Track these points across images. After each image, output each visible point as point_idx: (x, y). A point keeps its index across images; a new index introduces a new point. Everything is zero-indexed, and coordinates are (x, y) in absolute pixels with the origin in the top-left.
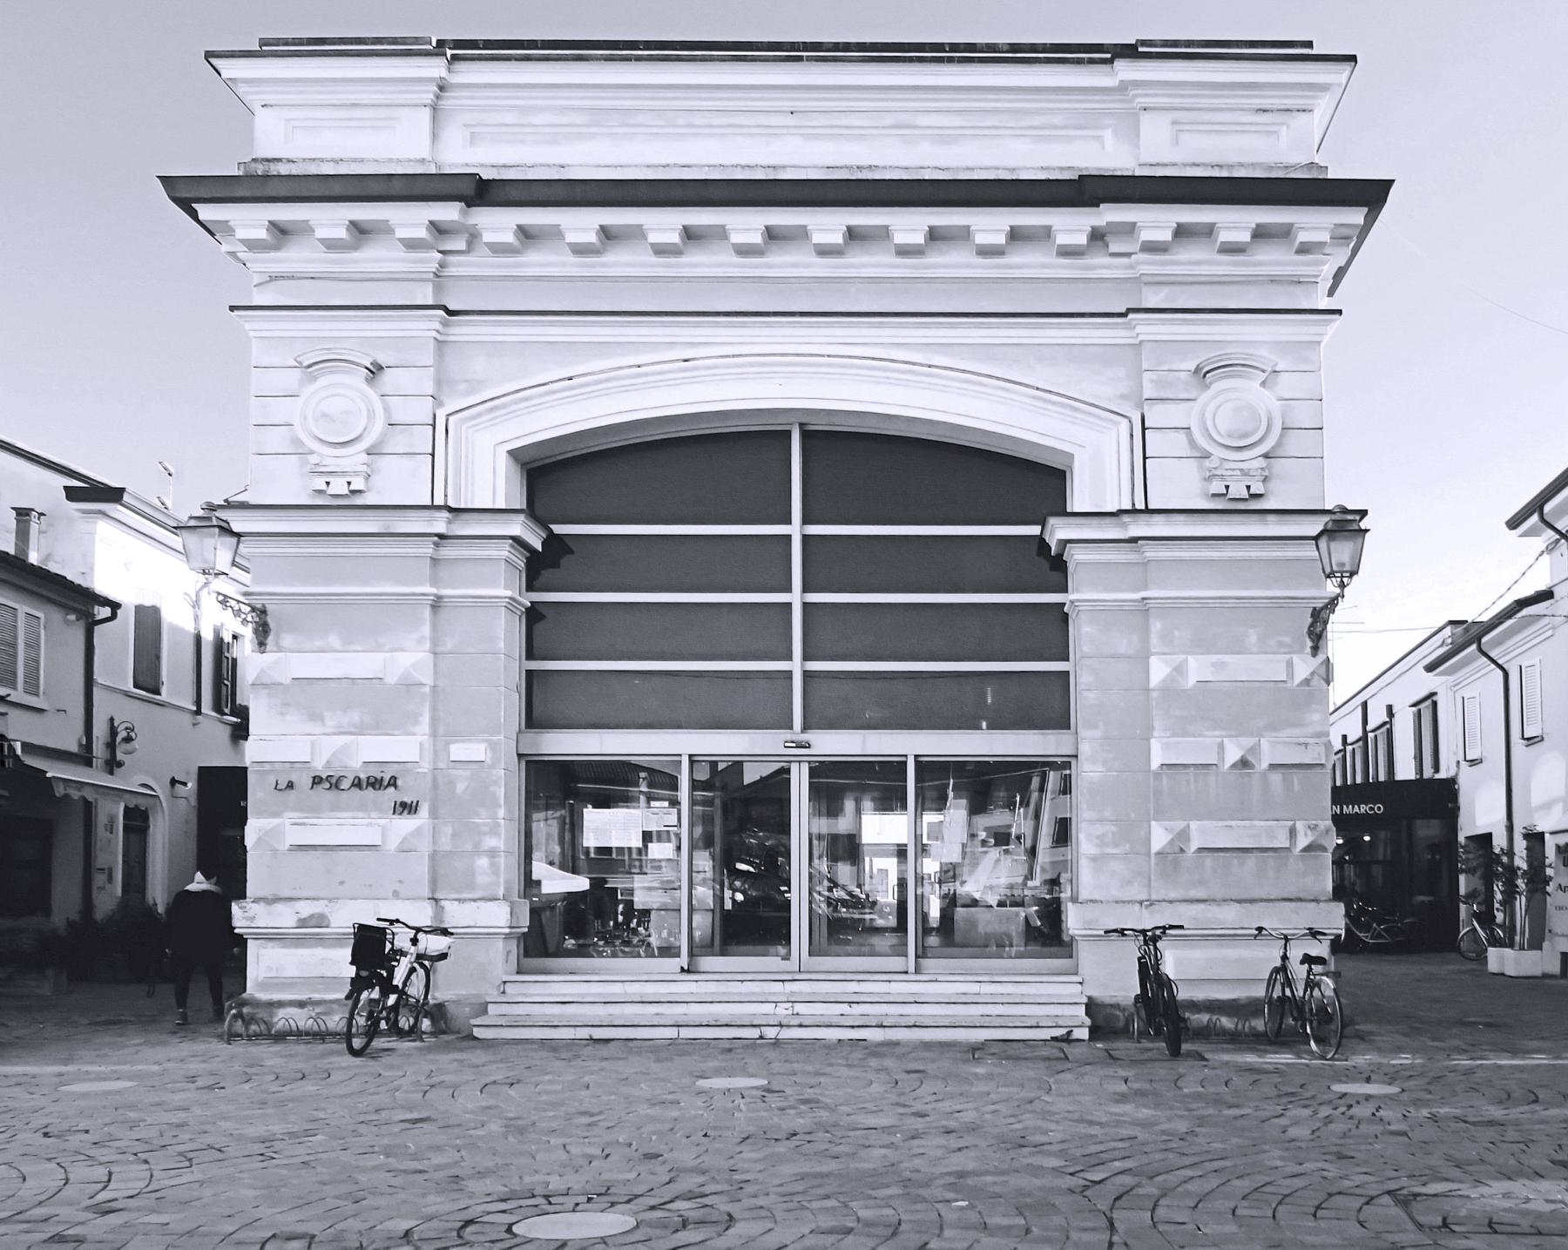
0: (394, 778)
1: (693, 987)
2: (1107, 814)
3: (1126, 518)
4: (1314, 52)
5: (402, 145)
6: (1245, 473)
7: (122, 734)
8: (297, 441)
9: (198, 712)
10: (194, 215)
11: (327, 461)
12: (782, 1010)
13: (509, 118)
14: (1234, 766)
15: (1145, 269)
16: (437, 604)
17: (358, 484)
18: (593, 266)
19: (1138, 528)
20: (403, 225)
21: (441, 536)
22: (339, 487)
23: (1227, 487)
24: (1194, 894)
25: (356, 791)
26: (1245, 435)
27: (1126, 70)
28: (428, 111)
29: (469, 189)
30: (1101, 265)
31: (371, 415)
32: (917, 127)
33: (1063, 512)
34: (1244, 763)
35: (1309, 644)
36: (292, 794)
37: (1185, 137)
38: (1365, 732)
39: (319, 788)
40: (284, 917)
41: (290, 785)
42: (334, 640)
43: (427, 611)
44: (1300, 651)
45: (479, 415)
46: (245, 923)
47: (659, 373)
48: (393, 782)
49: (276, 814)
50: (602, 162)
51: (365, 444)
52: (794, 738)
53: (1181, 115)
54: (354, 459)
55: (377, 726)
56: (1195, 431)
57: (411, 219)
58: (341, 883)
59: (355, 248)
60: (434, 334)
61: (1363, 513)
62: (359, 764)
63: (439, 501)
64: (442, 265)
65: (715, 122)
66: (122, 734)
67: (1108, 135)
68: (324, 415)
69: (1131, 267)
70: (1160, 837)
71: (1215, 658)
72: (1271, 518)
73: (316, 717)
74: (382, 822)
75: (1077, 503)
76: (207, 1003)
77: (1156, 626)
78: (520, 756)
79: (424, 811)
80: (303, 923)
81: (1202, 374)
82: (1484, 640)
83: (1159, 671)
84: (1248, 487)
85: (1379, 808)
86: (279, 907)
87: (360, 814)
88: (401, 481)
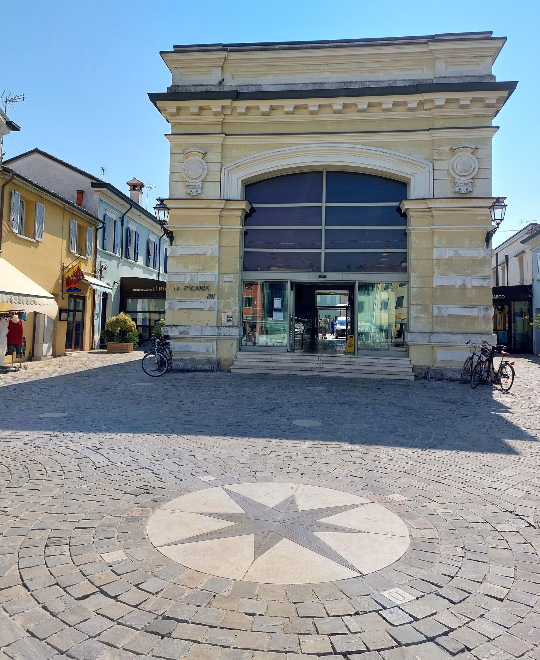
1: (291, 358)
2: (419, 302)
4: (493, 36)
6: (466, 184)
7: (104, 267)
9: (122, 258)
10: (156, 105)
17: (470, 189)
21: (222, 209)
25: (197, 292)
26: (466, 171)
27: (432, 46)
30: (422, 114)
31: (204, 168)
33: (406, 199)
36: (179, 291)
37: (449, 67)
38: (497, 266)
41: (178, 289)
42: (192, 242)
45: (234, 169)
47: (286, 154)
51: (201, 179)
52: (322, 274)
53: (448, 60)
54: (198, 182)
56: (450, 169)
57: (216, 105)
61: (505, 198)
65: (304, 69)
66: (104, 267)
67: (424, 67)
77: (436, 238)
79: (216, 298)
81: (452, 150)
83: (436, 254)
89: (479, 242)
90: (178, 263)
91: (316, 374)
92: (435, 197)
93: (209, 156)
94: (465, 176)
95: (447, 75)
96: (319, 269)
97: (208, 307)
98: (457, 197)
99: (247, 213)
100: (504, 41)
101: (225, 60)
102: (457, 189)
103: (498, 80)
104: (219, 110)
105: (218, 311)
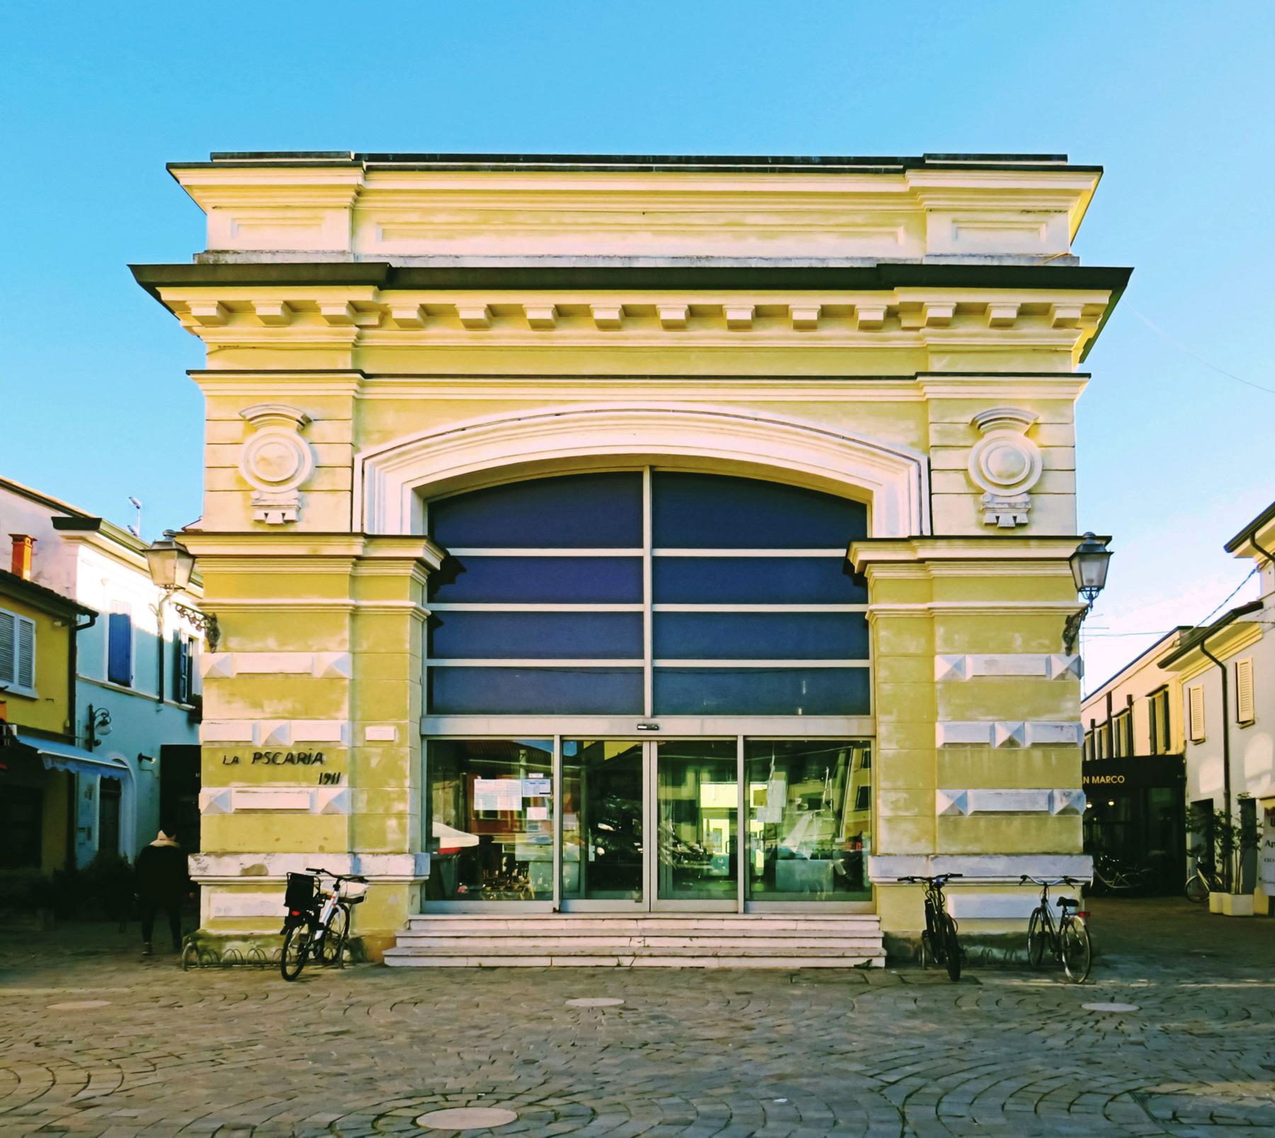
1: (563, 925)
2: (900, 784)
3: (915, 543)
5: (326, 239)
6: (1012, 506)
7: (99, 719)
8: (241, 480)
9: (161, 701)
10: (157, 296)
12: (635, 943)
13: (414, 217)
14: (1003, 745)
16: (355, 613)
17: (291, 515)
19: (925, 551)
21: (359, 558)
22: (275, 517)
24: (970, 848)
25: (289, 766)
26: (1012, 476)
27: (915, 179)
28: (347, 212)
29: (380, 275)
30: (895, 337)
31: (302, 458)
33: (863, 537)
34: (1011, 742)
35: (1064, 645)
37: (963, 233)
40: (231, 868)
41: (236, 760)
42: (271, 642)
43: (347, 620)
44: (1057, 651)
46: (199, 873)
47: (536, 425)
48: (319, 758)
49: (224, 784)
52: (646, 722)
53: (959, 215)
54: (288, 495)
55: (306, 712)
57: (334, 300)
58: (277, 840)
59: (289, 323)
60: (353, 393)
64: (359, 337)
66: (99, 719)
67: (901, 231)
68: (263, 459)
69: (919, 339)
70: (942, 803)
71: (987, 657)
72: (1033, 543)
73: (256, 705)
74: (311, 790)
75: (875, 531)
77: (940, 631)
78: (423, 736)
79: (344, 781)
80: (246, 872)
81: (977, 426)
82: (1207, 642)
83: (942, 667)
84: (1015, 518)
85: (1121, 779)
86: (226, 859)
87: (293, 784)
88: (327, 514)
89: (1047, 642)
90: (232, 695)
91: (627, 962)
92: (936, 533)
94: (1008, 486)
97: (319, 807)
98: (991, 534)
104: (343, 311)
105: (352, 818)
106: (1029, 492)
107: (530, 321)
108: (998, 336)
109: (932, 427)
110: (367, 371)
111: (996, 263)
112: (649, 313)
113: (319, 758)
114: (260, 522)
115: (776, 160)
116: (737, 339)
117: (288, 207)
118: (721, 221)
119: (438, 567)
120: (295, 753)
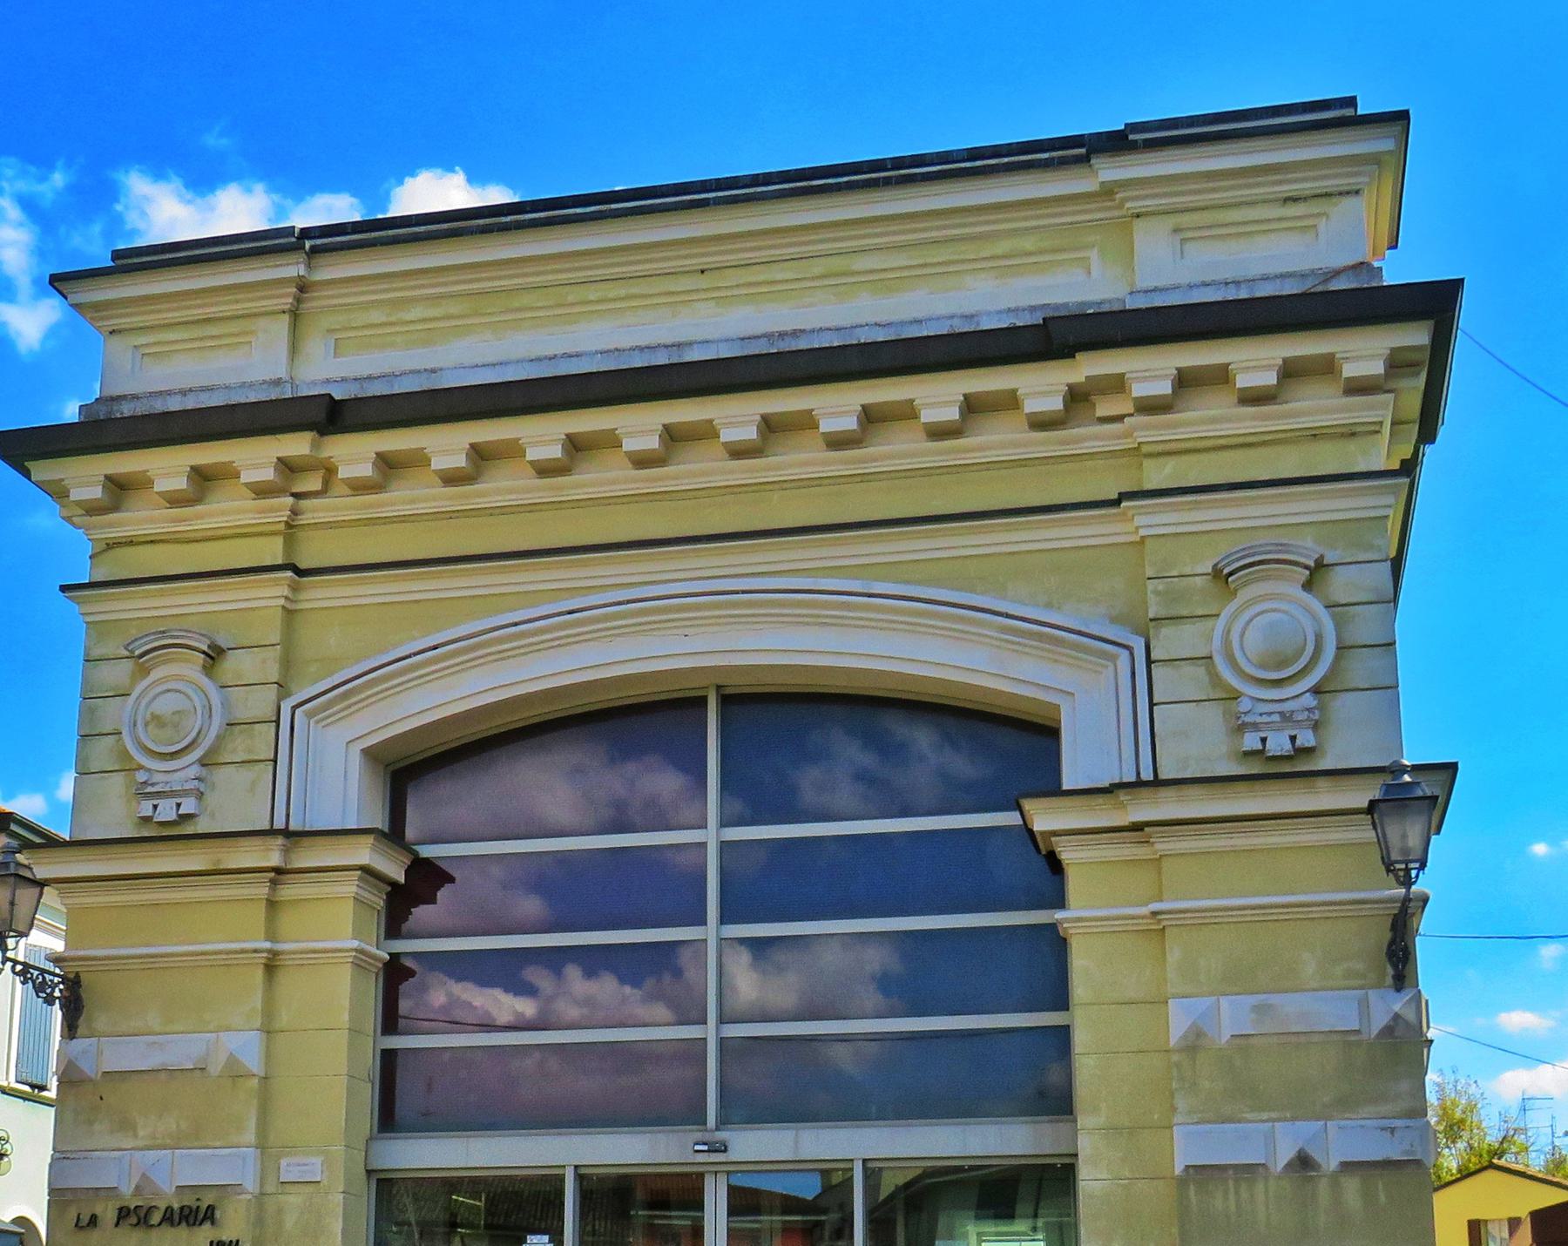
0: (211, 1208)
3: (1123, 796)
6: (1286, 717)
10: (27, 474)
11: (157, 778)
14: (1289, 1166)
15: (1141, 437)
17: (1306, 739)
18: (655, 480)
20: (630, 435)
21: (278, 871)
22: (167, 811)
23: (1264, 740)
27: (1109, 170)
28: (286, 317)
29: (320, 414)
30: (1087, 437)
32: (854, 273)
33: (1052, 789)
34: (1303, 1162)
35: (1390, 971)
37: (1188, 246)
39: (125, 1224)
43: (259, 974)
44: (1378, 985)
48: (209, 1215)
50: (479, 361)
51: (197, 754)
52: (707, 1137)
53: (1185, 220)
54: (184, 772)
56: (1218, 660)
57: (254, 458)
59: (115, 507)
60: (282, 602)
62: (1226, 1037)
63: (279, 824)
64: (295, 512)
67: (1093, 255)
68: (155, 717)
69: (1128, 434)
72: (1322, 783)
76: (1030, 1210)
77: (1174, 955)
78: (369, 1172)
84: (1293, 739)
88: (237, 801)
92: (1163, 776)
93: (232, 665)
94: (1278, 683)
95: (1185, 281)
96: (696, 1116)
99: (394, 884)
100: (1397, 128)
101: (303, 287)
102: (1251, 741)
103: (1388, 280)
104: (268, 474)
106: (1316, 691)
107: (629, 454)
108: (1254, 418)
109: (1151, 585)
110: (303, 565)
111: (1243, 295)
112: (704, 433)
113: (209, 1215)
114: (146, 820)
115: (898, 163)
116: (1156, 427)
117: (207, 321)
118: (817, 271)
119: (402, 880)
120: (176, 1206)
